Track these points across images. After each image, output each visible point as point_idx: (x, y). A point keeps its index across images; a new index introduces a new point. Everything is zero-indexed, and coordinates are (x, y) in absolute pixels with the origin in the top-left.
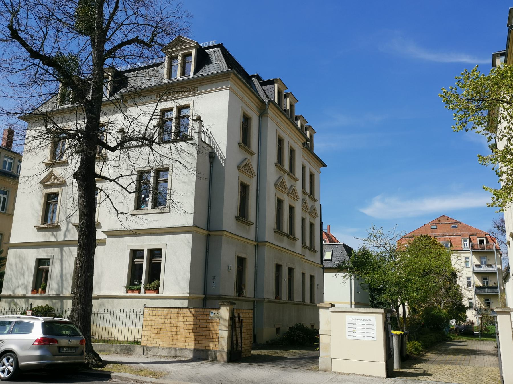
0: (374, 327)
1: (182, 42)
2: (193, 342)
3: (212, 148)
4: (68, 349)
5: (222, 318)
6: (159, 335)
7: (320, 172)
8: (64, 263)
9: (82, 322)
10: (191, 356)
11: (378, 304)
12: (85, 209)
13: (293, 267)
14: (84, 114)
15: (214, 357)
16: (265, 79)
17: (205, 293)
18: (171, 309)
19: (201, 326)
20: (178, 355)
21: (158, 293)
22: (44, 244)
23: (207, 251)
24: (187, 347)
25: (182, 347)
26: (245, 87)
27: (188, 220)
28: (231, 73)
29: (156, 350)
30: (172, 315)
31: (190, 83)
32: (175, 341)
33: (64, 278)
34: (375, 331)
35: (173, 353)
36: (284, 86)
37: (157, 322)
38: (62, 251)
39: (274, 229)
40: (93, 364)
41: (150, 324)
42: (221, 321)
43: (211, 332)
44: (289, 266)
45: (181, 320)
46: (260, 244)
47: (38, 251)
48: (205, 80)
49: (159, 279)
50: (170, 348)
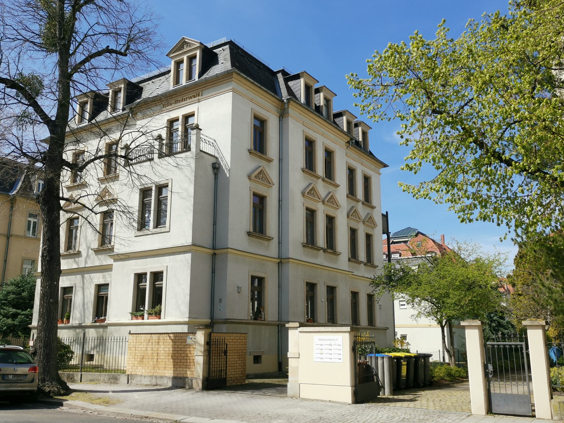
0: (341, 347)
1: (186, 43)
2: (172, 369)
3: (217, 158)
4: (14, 376)
5: (197, 343)
6: (141, 363)
7: (380, 174)
8: (85, 291)
9: (45, 350)
10: (170, 384)
11: (497, 327)
12: (47, 234)
13: (335, 286)
15: (190, 385)
16: (293, 73)
17: (212, 317)
18: (153, 335)
19: (179, 352)
20: (158, 384)
21: (160, 318)
22: (68, 271)
23: (213, 272)
24: (167, 375)
25: (162, 375)
26: (254, 86)
27: (186, 239)
28: (233, 72)
29: (139, 379)
30: (154, 341)
31: (193, 88)
32: (156, 368)
33: (86, 307)
34: (341, 352)
35: (154, 381)
36: (313, 79)
37: (140, 349)
38: (83, 277)
39: (302, 244)
40: (54, 393)
41: (134, 352)
42: (197, 347)
43: (188, 358)
44: (328, 285)
45: (162, 346)
46: (283, 261)
48: (208, 83)
49: (161, 305)
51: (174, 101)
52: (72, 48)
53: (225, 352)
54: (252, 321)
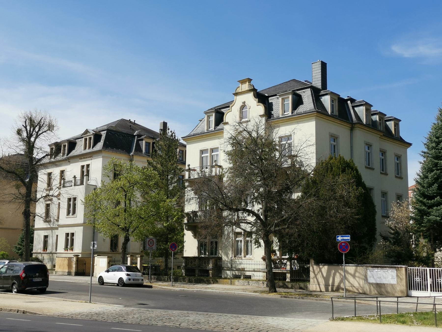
14: (259, 125)
38: (52, 232)
47: (44, 232)
50: (62, 272)
51: (83, 158)
52: (41, 129)
53: (85, 264)
54: (110, 252)
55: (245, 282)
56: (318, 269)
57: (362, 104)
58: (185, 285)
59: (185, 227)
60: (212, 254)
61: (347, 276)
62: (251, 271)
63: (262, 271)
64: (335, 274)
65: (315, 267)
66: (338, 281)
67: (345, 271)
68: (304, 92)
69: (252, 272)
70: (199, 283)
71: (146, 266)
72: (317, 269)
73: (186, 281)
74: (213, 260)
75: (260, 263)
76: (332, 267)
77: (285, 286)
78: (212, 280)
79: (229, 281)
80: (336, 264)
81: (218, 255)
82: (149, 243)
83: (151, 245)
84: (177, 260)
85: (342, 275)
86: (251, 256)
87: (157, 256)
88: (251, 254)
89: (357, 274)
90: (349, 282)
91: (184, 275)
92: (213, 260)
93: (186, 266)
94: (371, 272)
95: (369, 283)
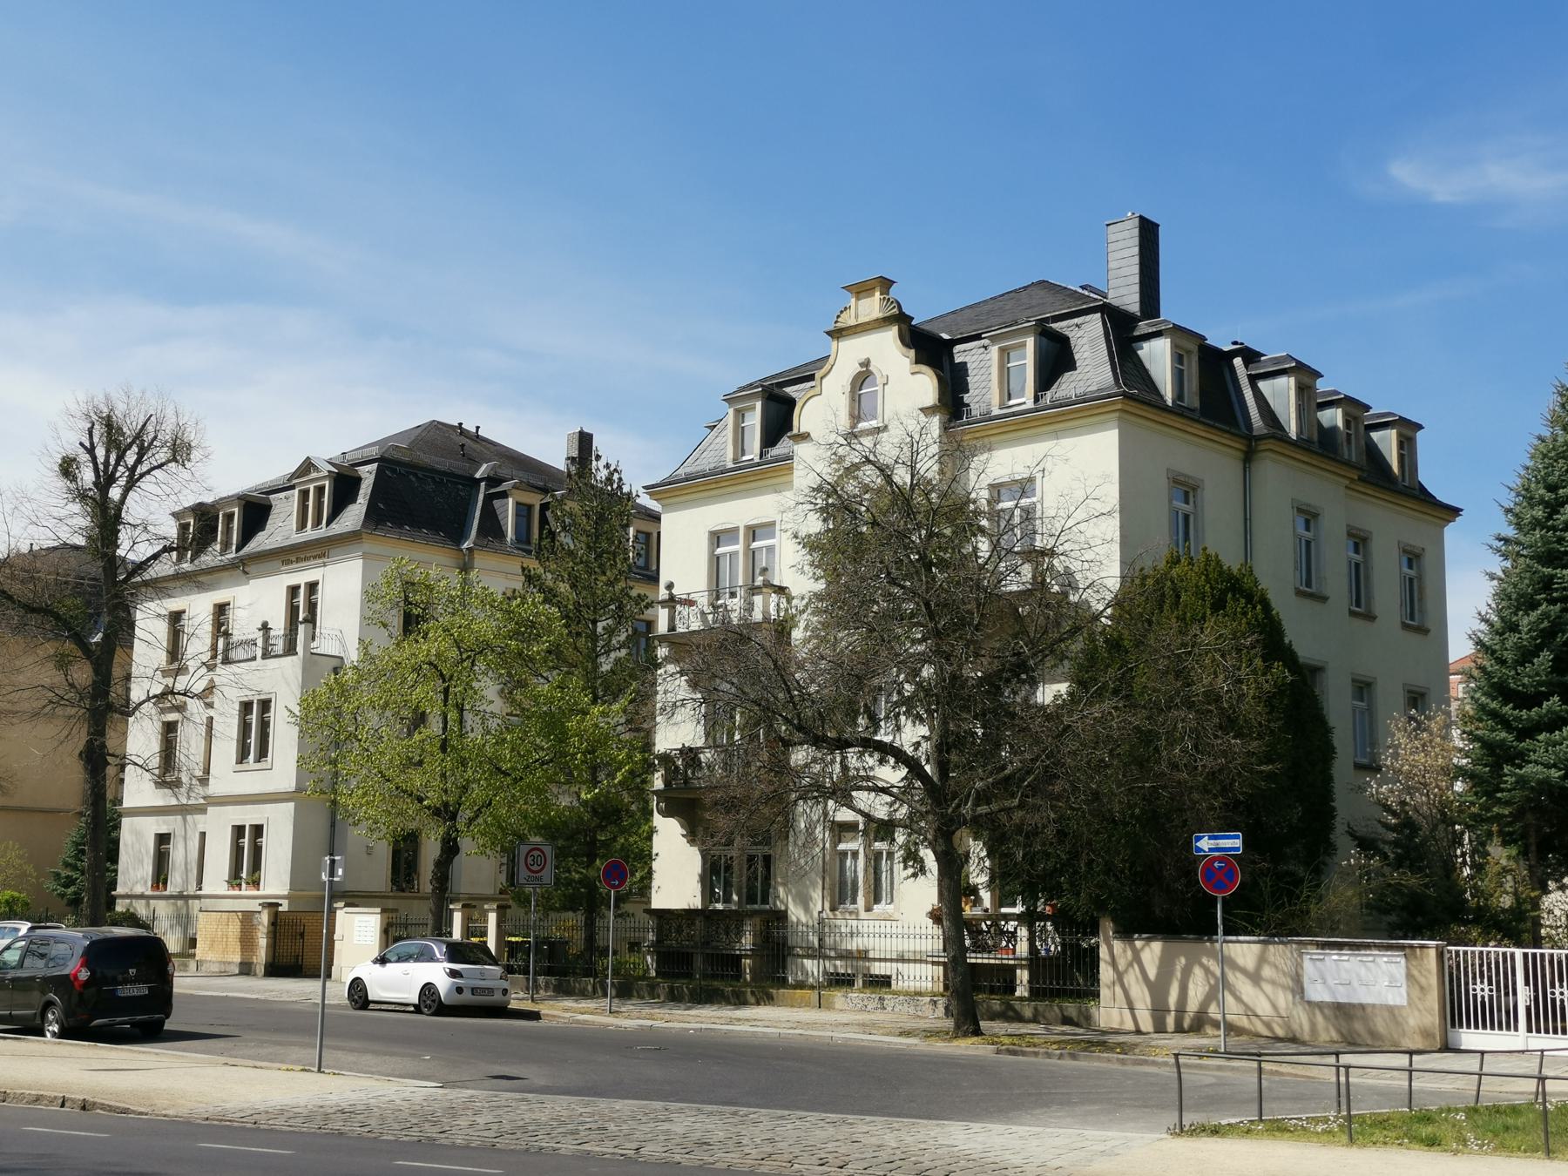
38: (185, 820)
47: (157, 821)
50: (220, 962)
51: (294, 559)
52: (145, 457)
53: (302, 935)
54: (391, 894)
55: (870, 998)
56: (1129, 953)
57: (1285, 369)
58: (657, 1011)
59: (657, 805)
60: (751, 899)
61: (1231, 976)
62: (891, 960)
63: (930, 959)
64: (1187, 972)
65: (1118, 945)
66: (1199, 995)
67: (1225, 961)
68: (1077, 325)
69: (894, 965)
70: (706, 1003)
71: (517, 942)
72: (1125, 951)
73: (659, 997)
74: (757, 920)
75: (924, 931)
76: (1177, 946)
77: (1011, 1013)
78: (753, 993)
79: (814, 995)
80: (1191, 936)
81: (775, 904)
82: (530, 860)
83: (535, 868)
84: (628, 919)
85: (1213, 975)
86: (892, 906)
87: (557, 905)
88: (892, 901)
89: (1267, 972)
90: (1238, 999)
91: (653, 973)
92: (757, 920)
93: (659, 941)
94: (1318, 963)
95: (1309, 1003)
